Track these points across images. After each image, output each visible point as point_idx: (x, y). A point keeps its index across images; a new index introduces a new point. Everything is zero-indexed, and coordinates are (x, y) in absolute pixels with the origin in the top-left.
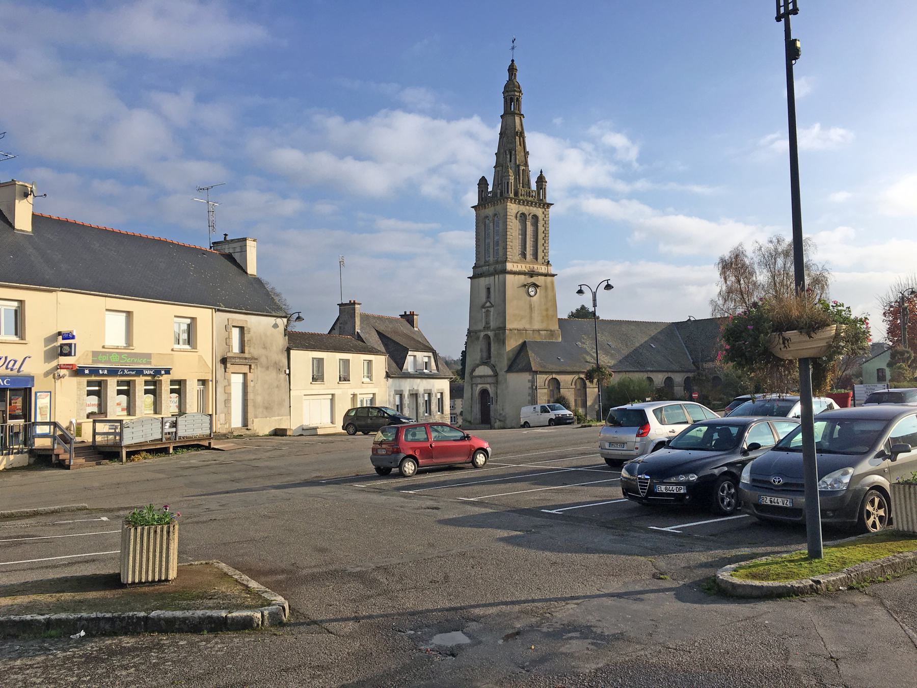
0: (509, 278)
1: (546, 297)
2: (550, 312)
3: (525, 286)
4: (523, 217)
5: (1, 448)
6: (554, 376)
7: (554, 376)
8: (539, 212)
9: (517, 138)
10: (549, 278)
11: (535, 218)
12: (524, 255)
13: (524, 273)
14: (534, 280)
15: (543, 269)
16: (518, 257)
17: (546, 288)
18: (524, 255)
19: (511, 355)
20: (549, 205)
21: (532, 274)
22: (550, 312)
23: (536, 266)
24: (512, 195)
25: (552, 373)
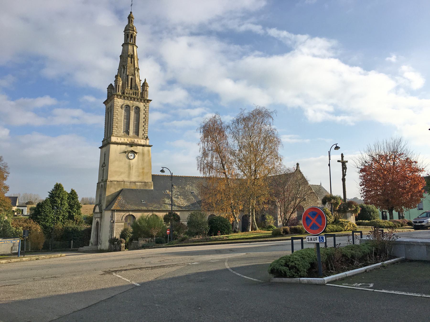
0: (112, 147)
1: (143, 160)
2: (146, 171)
3: (125, 152)
4: (128, 108)
5: (1, 233)
6: (131, 213)
7: (131, 213)
8: (141, 105)
9: (129, 59)
10: (146, 148)
11: (138, 109)
12: (127, 132)
13: (126, 144)
14: (133, 149)
15: (142, 142)
16: (122, 133)
17: (143, 154)
18: (127, 132)
19: (110, 199)
20: (149, 101)
21: (132, 145)
22: (146, 171)
23: (136, 140)
24: (120, 93)
25: (129, 211)
